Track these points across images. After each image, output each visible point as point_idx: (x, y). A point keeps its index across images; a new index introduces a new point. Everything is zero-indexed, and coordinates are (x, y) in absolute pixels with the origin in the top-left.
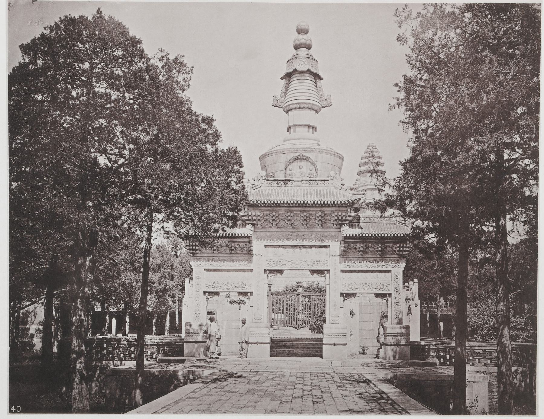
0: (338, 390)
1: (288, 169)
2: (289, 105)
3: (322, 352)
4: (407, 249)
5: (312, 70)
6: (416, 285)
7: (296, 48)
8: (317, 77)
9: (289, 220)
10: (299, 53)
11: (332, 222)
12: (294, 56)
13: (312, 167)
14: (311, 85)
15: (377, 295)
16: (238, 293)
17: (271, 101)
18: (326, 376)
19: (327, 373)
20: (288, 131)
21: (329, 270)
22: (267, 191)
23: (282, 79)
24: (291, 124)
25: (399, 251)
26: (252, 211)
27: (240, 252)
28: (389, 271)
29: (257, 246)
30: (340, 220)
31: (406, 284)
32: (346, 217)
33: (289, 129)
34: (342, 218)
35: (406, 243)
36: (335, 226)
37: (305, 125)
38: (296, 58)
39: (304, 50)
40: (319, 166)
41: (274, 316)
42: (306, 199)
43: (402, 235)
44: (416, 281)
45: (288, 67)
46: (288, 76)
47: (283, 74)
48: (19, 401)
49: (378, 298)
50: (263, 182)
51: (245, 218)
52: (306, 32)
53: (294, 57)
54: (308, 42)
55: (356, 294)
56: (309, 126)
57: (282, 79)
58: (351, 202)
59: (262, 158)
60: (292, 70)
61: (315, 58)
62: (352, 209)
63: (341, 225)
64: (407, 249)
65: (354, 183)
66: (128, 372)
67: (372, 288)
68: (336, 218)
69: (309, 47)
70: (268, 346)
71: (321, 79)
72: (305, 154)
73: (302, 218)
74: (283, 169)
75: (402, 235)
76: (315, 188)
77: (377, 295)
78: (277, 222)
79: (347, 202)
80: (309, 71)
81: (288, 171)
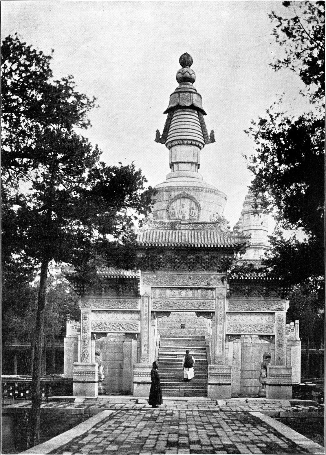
3: (206, 392)
6: (297, 326)
8: (201, 112)
14: (196, 122)
15: (261, 337)
18: (215, 414)
19: (214, 411)
20: (170, 168)
21: (215, 312)
23: (165, 113)
24: (174, 161)
27: (127, 294)
29: (143, 289)
44: (297, 322)
47: (165, 109)
48: (4, 452)
55: (240, 335)
56: (192, 163)
57: (165, 113)
58: (237, 245)
61: (198, 92)
63: (26, 170)
67: (256, 330)
70: (149, 386)
71: (205, 114)
77: (261, 337)
79: (233, 246)
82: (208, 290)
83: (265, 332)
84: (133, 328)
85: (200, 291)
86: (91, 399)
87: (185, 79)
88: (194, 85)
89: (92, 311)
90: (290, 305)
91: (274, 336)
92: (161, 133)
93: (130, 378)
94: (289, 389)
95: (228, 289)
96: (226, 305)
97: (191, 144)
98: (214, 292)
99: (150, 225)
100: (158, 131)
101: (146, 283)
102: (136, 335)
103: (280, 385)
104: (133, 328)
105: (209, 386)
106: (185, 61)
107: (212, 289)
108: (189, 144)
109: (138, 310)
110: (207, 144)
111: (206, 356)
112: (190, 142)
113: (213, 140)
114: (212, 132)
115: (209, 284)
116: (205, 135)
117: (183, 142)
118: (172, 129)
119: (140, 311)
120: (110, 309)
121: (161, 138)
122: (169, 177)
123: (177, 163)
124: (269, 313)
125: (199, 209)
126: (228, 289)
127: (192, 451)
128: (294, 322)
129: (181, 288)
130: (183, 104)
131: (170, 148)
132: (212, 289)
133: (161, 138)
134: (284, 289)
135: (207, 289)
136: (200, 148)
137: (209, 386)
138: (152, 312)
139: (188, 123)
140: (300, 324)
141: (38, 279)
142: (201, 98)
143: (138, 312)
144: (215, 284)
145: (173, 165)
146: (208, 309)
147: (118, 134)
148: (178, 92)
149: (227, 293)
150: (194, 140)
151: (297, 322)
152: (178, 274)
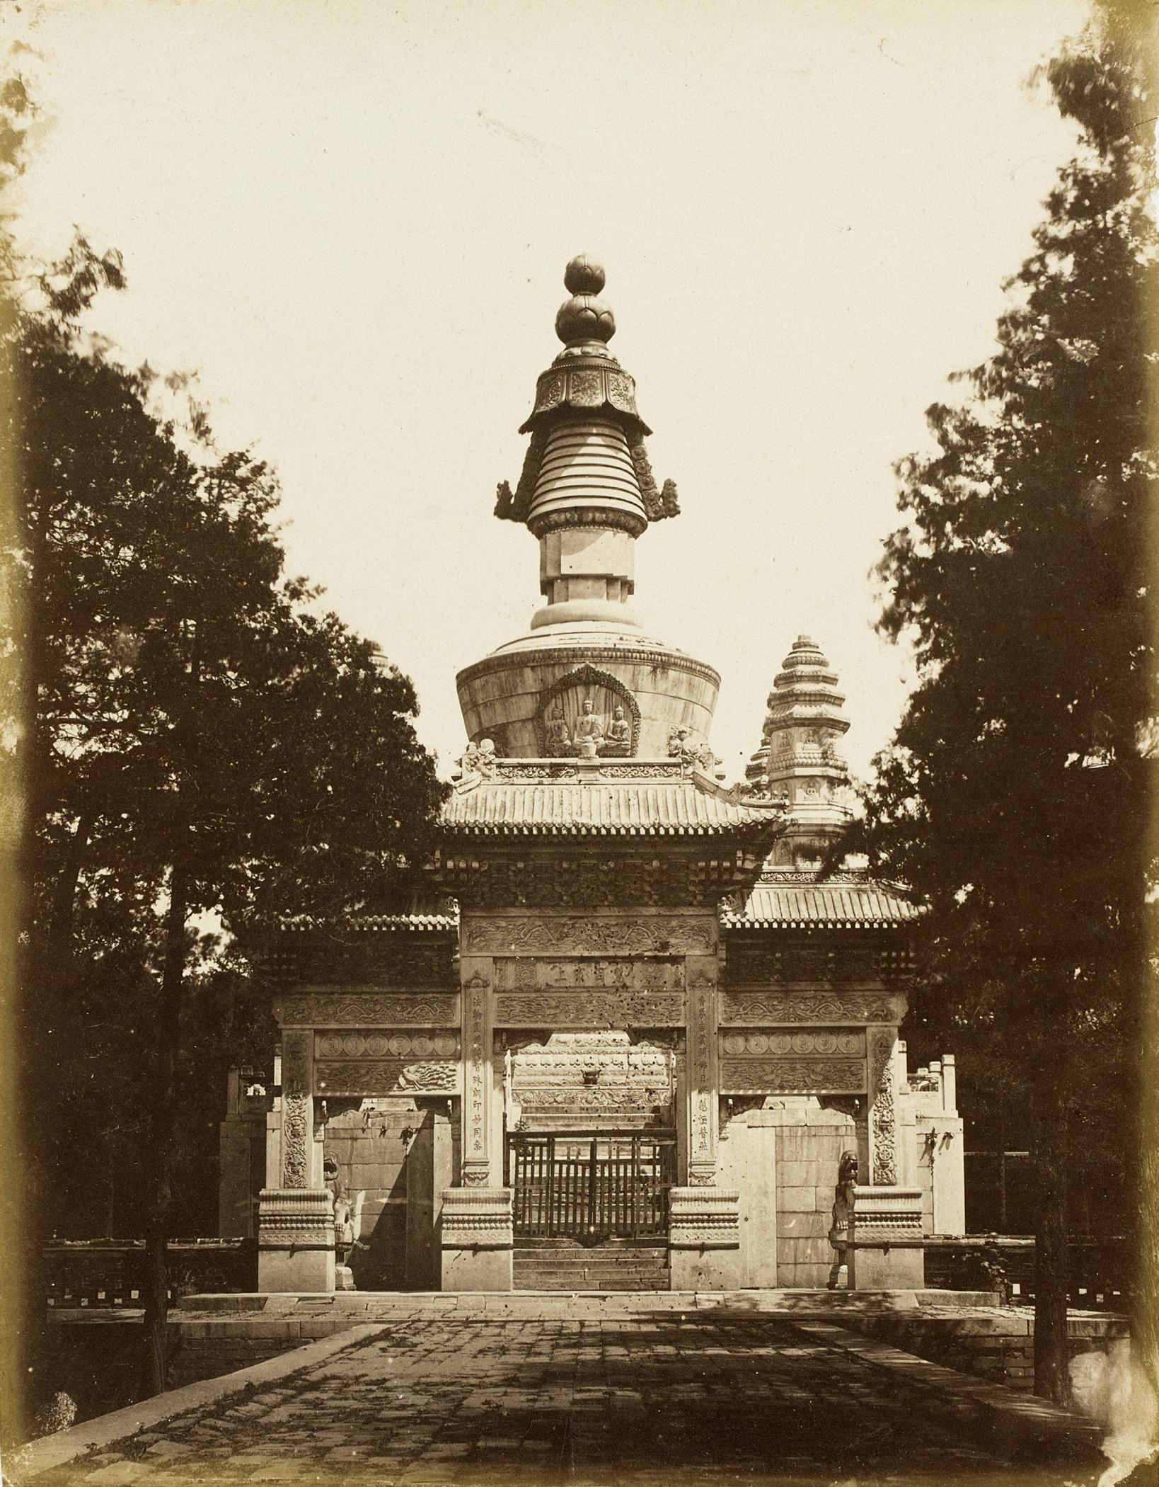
4: (911, 966)
6: (950, 1073)
9: (566, 883)
14: (622, 455)
16: (417, 1098)
22: (500, 797)
23: (522, 430)
25: (887, 971)
28: (862, 1030)
29: (471, 963)
30: (713, 882)
31: (922, 1072)
32: (732, 874)
34: (720, 876)
36: (700, 898)
37: (598, 577)
41: (484, 1169)
42: (615, 821)
43: (711, 832)
44: (949, 1059)
47: (525, 418)
49: (829, 1111)
57: (522, 430)
64: (911, 966)
66: (128, 1328)
68: (703, 877)
73: (602, 877)
75: (711, 832)
76: (641, 789)
78: (530, 889)
82: (664, 962)
84: (440, 1082)
85: (638, 966)
86: (314, 1298)
87: (581, 328)
88: (614, 348)
89: (317, 1032)
92: (513, 489)
93: (435, 1235)
94: (914, 1260)
95: (721, 960)
96: (717, 1006)
98: (681, 968)
99: (487, 772)
100: (504, 488)
102: (450, 1102)
104: (440, 1082)
106: (583, 280)
107: (675, 960)
109: (455, 1025)
110: (656, 520)
113: (673, 511)
114: (669, 485)
115: (665, 946)
116: (647, 499)
117: (581, 519)
118: (551, 448)
119: (459, 1030)
120: (371, 1026)
121: (516, 505)
122: (541, 621)
124: (827, 1028)
125: (635, 715)
126: (721, 960)
128: (939, 1059)
129: (582, 959)
130: (575, 409)
131: (540, 535)
132: (675, 960)
133: (516, 505)
134: (890, 955)
135: (658, 960)
138: (497, 1032)
139: (594, 472)
140: (957, 1066)
143: (456, 1032)
144: (680, 944)
145: (552, 584)
147: (401, 566)
148: (564, 370)
149: (720, 971)
151: (949, 1059)
152: (571, 918)
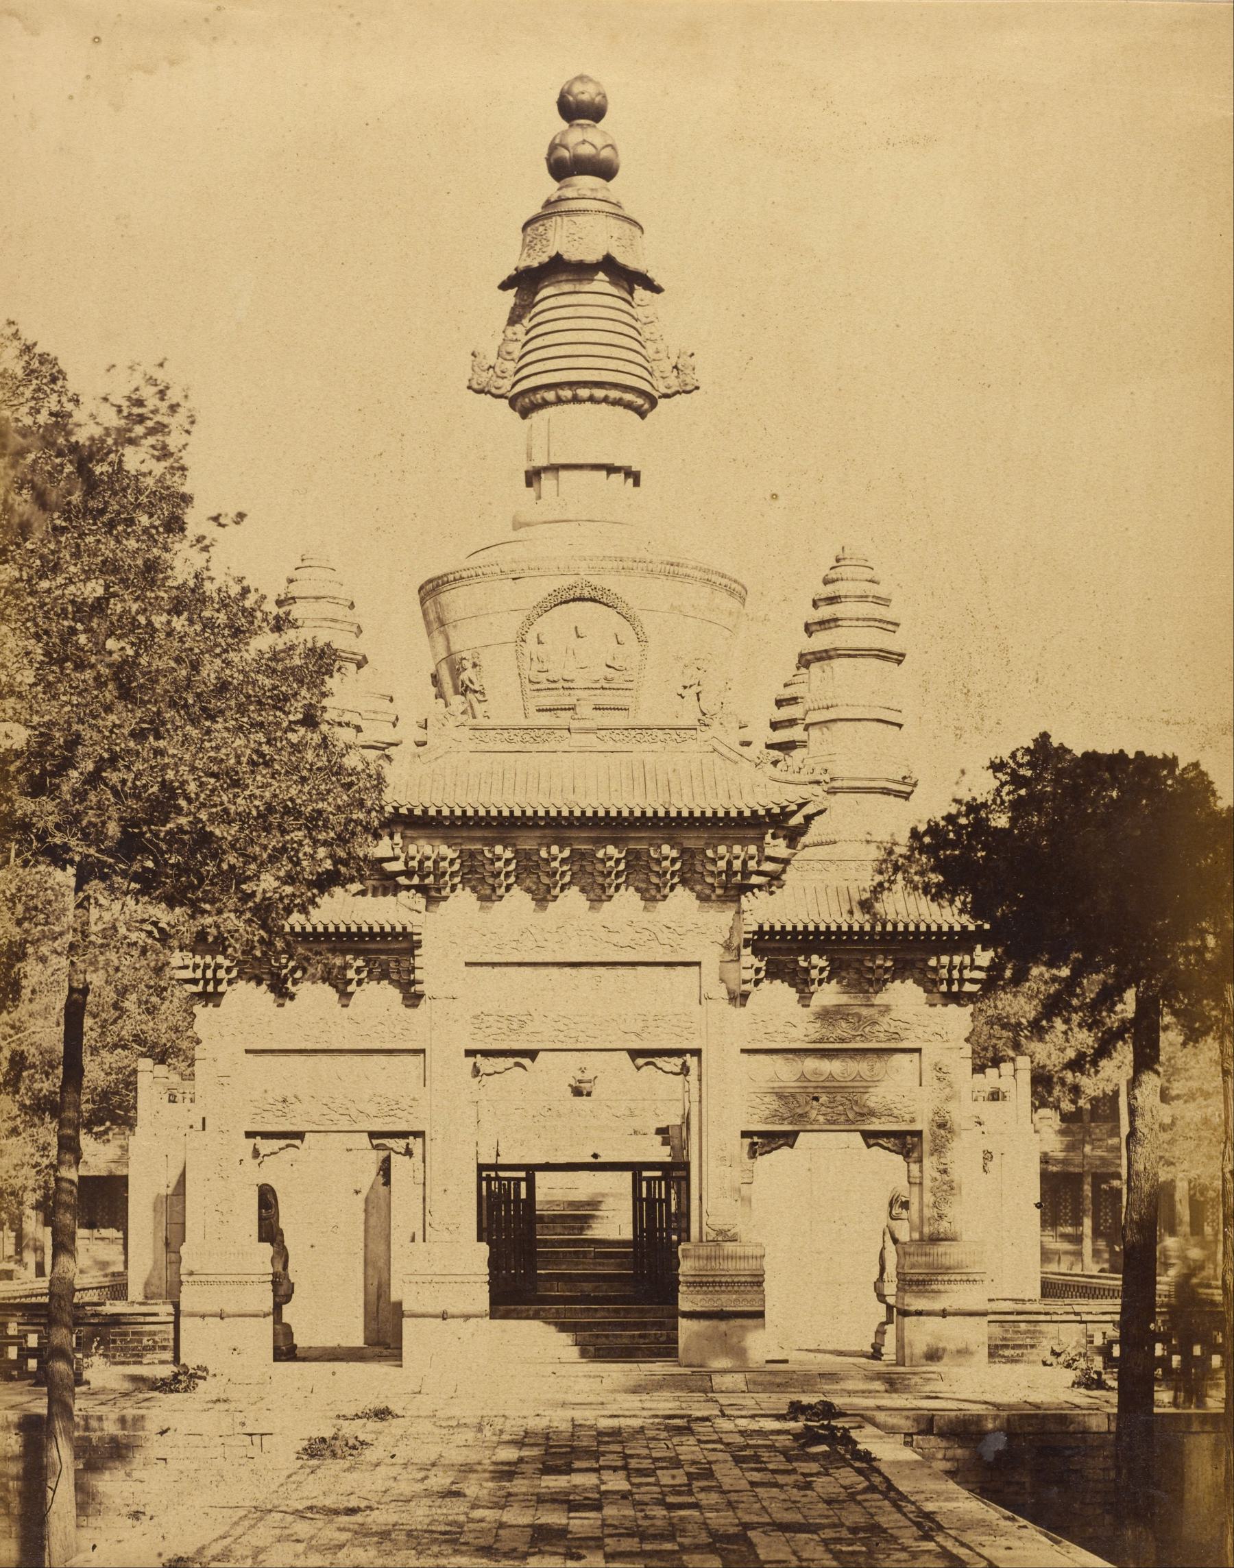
0: (737, 1471)
1: (531, 637)
2: (535, 389)
5: (621, 259)
7: (561, 169)
10: (568, 193)
11: (709, 880)
12: (548, 203)
13: (627, 632)
17: (463, 372)
20: (529, 484)
23: (504, 286)
24: (541, 462)
26: (422, 842)
33: (533, 477)
35: (970, 951)
36: (719, 891)
38: (560, 214)
39: (586, 182)
40: (649, 624)
45: (527, 246)
46: (526, 282)
50: (456, 734)
51: (397, 866)
52: (595, 112)
53: (551, 208)
54: (606, 153)
57: (504, 286)
59: (431, 590)
60: (544, 258)
61: (627, 212)
62: (781, 833)
65: (788, 678)
67: (851, 1116)
69: (606, 171)
72: (595, 581)
74: (512, 636)
80: (609, 265)
81: (531, 646)
83: (883, 1119)
90: (919, 985)
91: (919, 1134)
97: (576, 399)
101: (452, 929)
103: (700, 1102)
105: (683, 1323)
108: (568, 402)
111: (701, 1241)
112: (567, 393)
123: (555, 468)
127: (610, 1557)
136: (642, 415)
137: (683, 1323)
141: (102, 1128)
142: (641, 228)
146: (1023, 1326)
150: (615, 386)
